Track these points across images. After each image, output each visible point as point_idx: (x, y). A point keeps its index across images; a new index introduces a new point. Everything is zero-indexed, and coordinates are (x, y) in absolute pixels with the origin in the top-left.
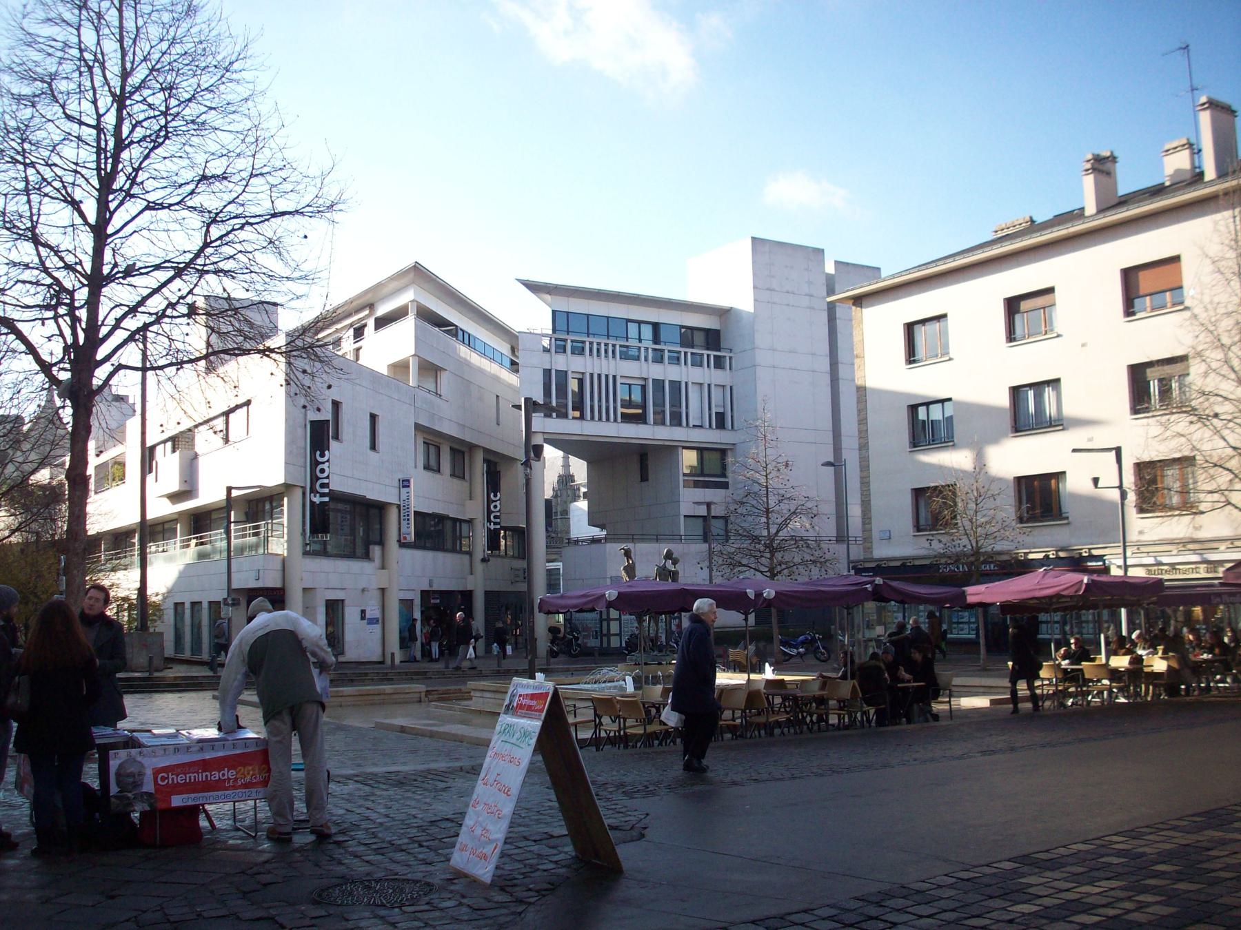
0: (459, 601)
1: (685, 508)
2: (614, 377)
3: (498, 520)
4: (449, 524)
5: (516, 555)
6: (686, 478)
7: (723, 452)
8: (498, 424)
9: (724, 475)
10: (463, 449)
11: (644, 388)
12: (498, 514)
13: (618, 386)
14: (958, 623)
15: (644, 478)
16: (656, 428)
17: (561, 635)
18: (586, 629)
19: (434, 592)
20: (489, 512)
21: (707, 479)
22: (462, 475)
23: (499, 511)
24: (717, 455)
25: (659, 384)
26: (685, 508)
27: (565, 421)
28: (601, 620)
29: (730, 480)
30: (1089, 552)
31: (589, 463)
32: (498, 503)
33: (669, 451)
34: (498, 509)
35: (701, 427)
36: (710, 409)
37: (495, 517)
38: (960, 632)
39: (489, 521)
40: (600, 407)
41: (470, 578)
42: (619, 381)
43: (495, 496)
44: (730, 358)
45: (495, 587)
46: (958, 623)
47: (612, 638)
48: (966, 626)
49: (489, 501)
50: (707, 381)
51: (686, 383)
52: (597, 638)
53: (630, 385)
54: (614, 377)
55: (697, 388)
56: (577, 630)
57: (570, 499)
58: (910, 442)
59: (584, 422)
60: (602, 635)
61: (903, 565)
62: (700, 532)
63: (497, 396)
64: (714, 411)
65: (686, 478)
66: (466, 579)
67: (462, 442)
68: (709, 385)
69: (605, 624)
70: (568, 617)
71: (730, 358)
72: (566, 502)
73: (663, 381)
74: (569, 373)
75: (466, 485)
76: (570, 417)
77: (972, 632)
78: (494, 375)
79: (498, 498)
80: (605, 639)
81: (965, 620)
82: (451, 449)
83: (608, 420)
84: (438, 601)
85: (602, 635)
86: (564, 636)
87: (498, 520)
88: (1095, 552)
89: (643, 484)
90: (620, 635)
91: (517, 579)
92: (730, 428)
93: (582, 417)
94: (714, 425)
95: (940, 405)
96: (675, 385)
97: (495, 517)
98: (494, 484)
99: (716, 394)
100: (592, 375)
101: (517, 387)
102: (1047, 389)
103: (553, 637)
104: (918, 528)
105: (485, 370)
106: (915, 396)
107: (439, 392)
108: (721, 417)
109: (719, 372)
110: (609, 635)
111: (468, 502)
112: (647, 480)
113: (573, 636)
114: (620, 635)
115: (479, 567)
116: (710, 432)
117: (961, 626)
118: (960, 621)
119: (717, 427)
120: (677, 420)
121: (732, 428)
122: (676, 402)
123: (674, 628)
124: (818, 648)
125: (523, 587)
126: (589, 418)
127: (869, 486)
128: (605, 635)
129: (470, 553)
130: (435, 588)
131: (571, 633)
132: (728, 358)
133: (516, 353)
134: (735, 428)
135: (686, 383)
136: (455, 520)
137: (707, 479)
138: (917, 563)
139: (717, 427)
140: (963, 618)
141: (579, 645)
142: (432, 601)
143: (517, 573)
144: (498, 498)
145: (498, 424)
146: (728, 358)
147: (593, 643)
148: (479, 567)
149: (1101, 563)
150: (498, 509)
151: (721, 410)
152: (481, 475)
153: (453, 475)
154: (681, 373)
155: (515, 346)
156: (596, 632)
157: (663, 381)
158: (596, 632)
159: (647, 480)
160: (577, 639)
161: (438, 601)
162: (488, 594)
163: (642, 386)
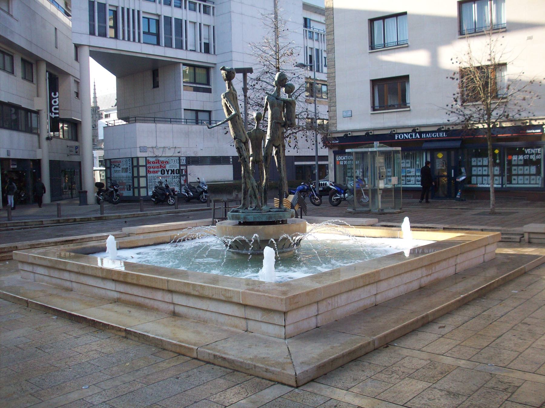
0: (32, 167)
1: (185, 105)
2: (139, 12)
3: (57, 111)
4: (22, 114)
5: (70, 138)
6: (185, 84)
7: (207, 69)
8: (56, 47)
9: (208, 83)
10: (32, 61)
11: (158, 22)
12: (57, 107)
13: (141, 19)
14: (406, 176)
15: (156, 85)
16: (166, 48)
17: (104, 188)
18: (123, 184)
19: (14, 160)
20: (51, 106)
21: (198, 86)
22: (31, 80)
23: (58, 105)
24: (204, 72)
25: (168, 20)
26: (185, 105)
27: (105, 38)
28: (133, 177)
29: (212, 87)
30: (530, 122)
31: (118, 78)
32: (57, 100)
33: (173, 65)
34: (57, 104)
35: (195, 51)
36: (200, 40)
37: (55, 109)
38: (407, 183)
39: (51, 111)
40: (129, 26)
41: (39, 151)
42: (142, 15)
43: (55, 94)
44: (213, 8)
45: (57, 157)
46: (406, 176)
47: (141, 190)
48: (413, 179)
49: (51, 98)
50: (199, 21)
51: (186, 21)
52: (130, 190)
53: (149, 19)
54: (139, 12)
55: (192, 25)
56: (116, 185)
57: (97, 119)
58: (370, 46)
59: (118, 41)
60: (134, 188)
61: (346, 135)
62: (194, 118)
63: (56, 29)
64: (203, 41)
65: (185, 84)
66: (35, 151)
67: (31, 54)
68: (200, 24)
69: (136, 180)
70: (183, 178)
71: (213, 8)
72: (95, 121)
73: (171, 18)
74: (107, 5)
75: (35, 86)
76: (108, 36)
77: (417, 183)
78: (53, 13)
79: (57, 96)
80: (136, 191)
81: (412, 174)
82: (23, 60)
83: (134, 40)
84: (16, 167)
85: (134, 188)
86: (107, 190)
87: (57, 111)
88: (534, 123)
89: (155, 89)
90: (146, 187)
91: (71, 153)
92: (213, 53)
93: (116, 37)
94: (203, 51)
95: (381, 21)
96: (179, 22)
97: (55, 109)
98: (54, 86)
99: (204, 30)
100: (123, 8)
101: (69, 27)
102: (473, 5)
103: (99, 190)
104: (374, 109)
105: (47, 8)
106: (370, 12)
107: (11, 13)
108: (207, 46)
109: (206, 16)
110: (139, 188)
111: (36, 99)
112: (158, 86)
113: (114, 189)
114: (146, 187)
115: (45, 143)
116: (200, 54)
117: (408, 178)
118: (408, 174)
119: (205, 52)
120: (179, 46)
121: (214, 53)
122: (179, 32)
123: (183, 182)
124: (313, 195)
125: (76, 158)
126: (121, 38)
127: (335, 79)
128: (136, 188)
129: (39, 135)
130: (12, 156)
131: (113, 185)
132: (212, 8)
133: (68, 7)
134: (216, 53)
135: (186, 21)
136: (27, 111)
137: (198, 86)
138: (376, 133)
139: (205, 52)
140: (410, 172)
141: (118, 195)
142: (11, 167)
143: (71, 149)
144: (57, 96)
145: (56, 47)
146: (212, 8)
147: (126, 193)
148: (45, 143)
149: (539, 131)
150: (57, 104)
151: (207, 41)
152: (45, 80)
153: (24, 78)
154: (182, 14)
155: (68, 2)
156: (130, 186)
157: (171, 18)
158: (130, 186)
159: (158, 86)
160: (116, 191)
161: (16, 167)
162: (51, 162)
163: (156, 20)
